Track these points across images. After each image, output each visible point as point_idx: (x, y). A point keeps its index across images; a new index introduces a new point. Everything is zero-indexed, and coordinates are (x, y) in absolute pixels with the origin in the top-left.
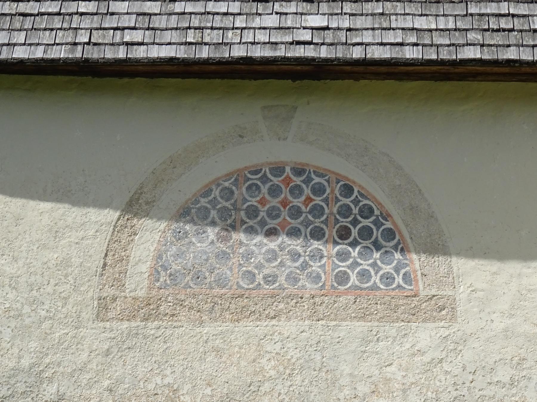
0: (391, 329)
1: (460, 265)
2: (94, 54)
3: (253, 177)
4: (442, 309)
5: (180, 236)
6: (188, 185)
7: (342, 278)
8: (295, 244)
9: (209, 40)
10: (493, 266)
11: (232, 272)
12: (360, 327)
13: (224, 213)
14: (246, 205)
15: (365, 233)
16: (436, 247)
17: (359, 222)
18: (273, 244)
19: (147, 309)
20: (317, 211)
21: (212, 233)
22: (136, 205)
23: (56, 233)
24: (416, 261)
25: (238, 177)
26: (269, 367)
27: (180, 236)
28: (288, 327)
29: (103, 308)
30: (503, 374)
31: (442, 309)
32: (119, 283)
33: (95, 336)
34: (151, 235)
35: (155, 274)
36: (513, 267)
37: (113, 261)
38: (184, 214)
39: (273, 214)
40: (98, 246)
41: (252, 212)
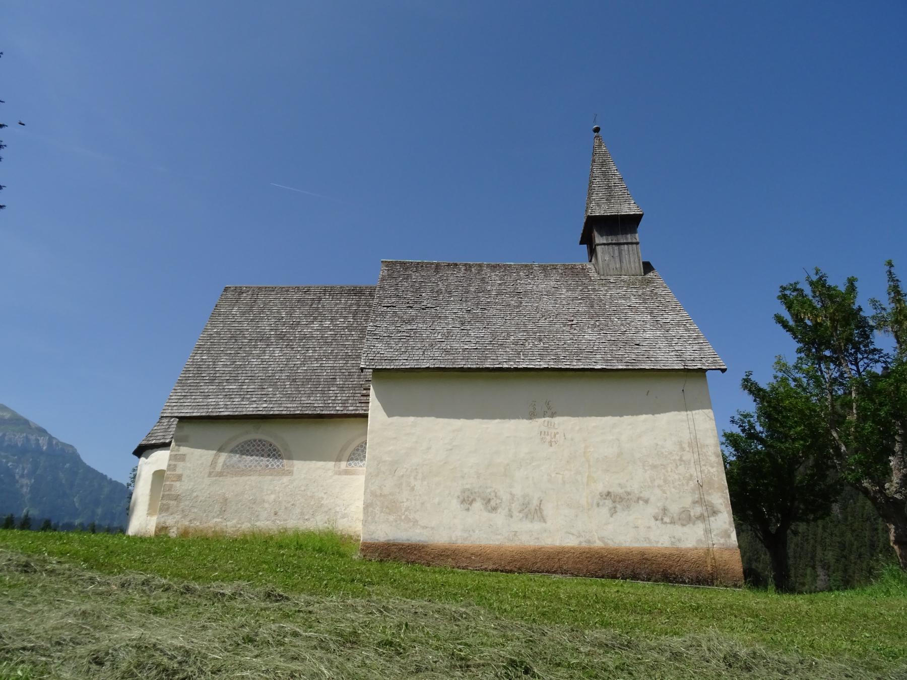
0: (277, 478)
1: (295, 462)
2: (212, 414)
3: (249, 443)
4: (290, 473)
5: (230, 457)
6: (233, 445)
7: (267, 466)
8: (257, 458)
9: (356, 507)
10: (302, 462)
11: (241, 465)
12: (270, 477)
13: (241, 451)
14: (245, 449)
15: (274, 455)
16: (290, 458)
17: (273, 453)
18: (252, 458)
19: (220, 474)
20: (263, 450)
21: (238, 456)
22: (220, 450)
23: (201, 457)
24: (285, 461)
25: (246, 442)
26: (247, 487)
27: (230, 457)
28: (253, 478)
29: (210, 474)
30: (303, 488)
31: (290, 473)
32: (214, 468)
33: (207, 481)
34: (223, 456)
35: (223, 466)
36: (308, 462)
37: (214, 463)
38: (232, 451)
39: (253, 451)
40: (211, 459)
41: (248, 451)
